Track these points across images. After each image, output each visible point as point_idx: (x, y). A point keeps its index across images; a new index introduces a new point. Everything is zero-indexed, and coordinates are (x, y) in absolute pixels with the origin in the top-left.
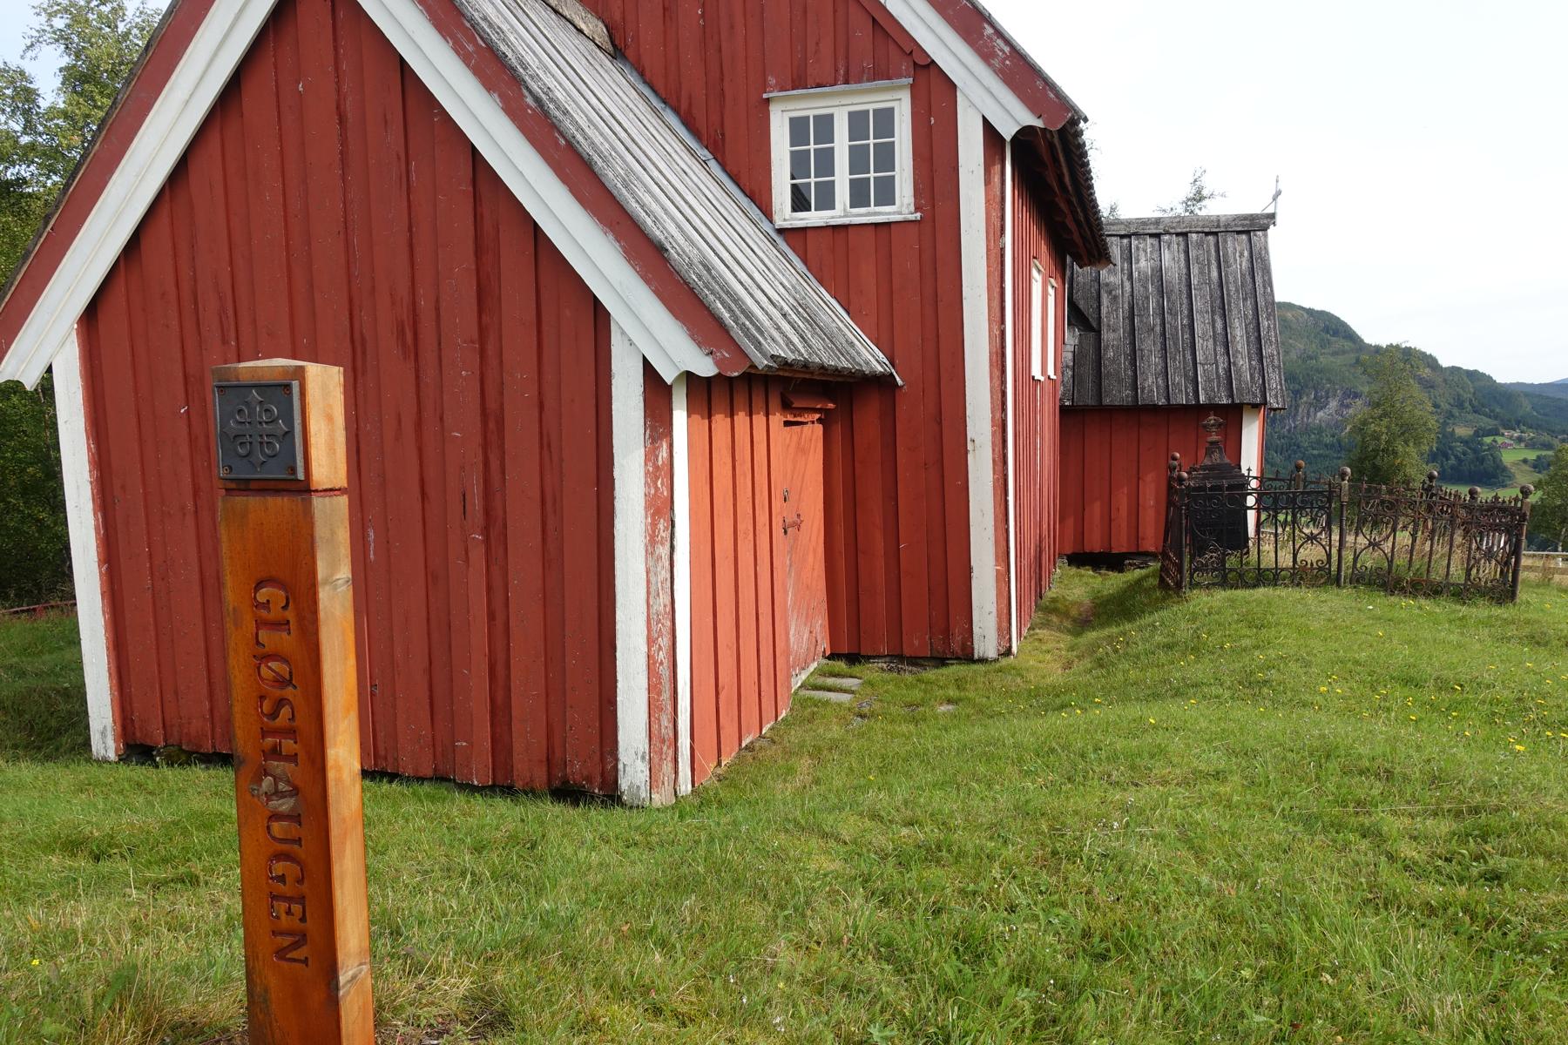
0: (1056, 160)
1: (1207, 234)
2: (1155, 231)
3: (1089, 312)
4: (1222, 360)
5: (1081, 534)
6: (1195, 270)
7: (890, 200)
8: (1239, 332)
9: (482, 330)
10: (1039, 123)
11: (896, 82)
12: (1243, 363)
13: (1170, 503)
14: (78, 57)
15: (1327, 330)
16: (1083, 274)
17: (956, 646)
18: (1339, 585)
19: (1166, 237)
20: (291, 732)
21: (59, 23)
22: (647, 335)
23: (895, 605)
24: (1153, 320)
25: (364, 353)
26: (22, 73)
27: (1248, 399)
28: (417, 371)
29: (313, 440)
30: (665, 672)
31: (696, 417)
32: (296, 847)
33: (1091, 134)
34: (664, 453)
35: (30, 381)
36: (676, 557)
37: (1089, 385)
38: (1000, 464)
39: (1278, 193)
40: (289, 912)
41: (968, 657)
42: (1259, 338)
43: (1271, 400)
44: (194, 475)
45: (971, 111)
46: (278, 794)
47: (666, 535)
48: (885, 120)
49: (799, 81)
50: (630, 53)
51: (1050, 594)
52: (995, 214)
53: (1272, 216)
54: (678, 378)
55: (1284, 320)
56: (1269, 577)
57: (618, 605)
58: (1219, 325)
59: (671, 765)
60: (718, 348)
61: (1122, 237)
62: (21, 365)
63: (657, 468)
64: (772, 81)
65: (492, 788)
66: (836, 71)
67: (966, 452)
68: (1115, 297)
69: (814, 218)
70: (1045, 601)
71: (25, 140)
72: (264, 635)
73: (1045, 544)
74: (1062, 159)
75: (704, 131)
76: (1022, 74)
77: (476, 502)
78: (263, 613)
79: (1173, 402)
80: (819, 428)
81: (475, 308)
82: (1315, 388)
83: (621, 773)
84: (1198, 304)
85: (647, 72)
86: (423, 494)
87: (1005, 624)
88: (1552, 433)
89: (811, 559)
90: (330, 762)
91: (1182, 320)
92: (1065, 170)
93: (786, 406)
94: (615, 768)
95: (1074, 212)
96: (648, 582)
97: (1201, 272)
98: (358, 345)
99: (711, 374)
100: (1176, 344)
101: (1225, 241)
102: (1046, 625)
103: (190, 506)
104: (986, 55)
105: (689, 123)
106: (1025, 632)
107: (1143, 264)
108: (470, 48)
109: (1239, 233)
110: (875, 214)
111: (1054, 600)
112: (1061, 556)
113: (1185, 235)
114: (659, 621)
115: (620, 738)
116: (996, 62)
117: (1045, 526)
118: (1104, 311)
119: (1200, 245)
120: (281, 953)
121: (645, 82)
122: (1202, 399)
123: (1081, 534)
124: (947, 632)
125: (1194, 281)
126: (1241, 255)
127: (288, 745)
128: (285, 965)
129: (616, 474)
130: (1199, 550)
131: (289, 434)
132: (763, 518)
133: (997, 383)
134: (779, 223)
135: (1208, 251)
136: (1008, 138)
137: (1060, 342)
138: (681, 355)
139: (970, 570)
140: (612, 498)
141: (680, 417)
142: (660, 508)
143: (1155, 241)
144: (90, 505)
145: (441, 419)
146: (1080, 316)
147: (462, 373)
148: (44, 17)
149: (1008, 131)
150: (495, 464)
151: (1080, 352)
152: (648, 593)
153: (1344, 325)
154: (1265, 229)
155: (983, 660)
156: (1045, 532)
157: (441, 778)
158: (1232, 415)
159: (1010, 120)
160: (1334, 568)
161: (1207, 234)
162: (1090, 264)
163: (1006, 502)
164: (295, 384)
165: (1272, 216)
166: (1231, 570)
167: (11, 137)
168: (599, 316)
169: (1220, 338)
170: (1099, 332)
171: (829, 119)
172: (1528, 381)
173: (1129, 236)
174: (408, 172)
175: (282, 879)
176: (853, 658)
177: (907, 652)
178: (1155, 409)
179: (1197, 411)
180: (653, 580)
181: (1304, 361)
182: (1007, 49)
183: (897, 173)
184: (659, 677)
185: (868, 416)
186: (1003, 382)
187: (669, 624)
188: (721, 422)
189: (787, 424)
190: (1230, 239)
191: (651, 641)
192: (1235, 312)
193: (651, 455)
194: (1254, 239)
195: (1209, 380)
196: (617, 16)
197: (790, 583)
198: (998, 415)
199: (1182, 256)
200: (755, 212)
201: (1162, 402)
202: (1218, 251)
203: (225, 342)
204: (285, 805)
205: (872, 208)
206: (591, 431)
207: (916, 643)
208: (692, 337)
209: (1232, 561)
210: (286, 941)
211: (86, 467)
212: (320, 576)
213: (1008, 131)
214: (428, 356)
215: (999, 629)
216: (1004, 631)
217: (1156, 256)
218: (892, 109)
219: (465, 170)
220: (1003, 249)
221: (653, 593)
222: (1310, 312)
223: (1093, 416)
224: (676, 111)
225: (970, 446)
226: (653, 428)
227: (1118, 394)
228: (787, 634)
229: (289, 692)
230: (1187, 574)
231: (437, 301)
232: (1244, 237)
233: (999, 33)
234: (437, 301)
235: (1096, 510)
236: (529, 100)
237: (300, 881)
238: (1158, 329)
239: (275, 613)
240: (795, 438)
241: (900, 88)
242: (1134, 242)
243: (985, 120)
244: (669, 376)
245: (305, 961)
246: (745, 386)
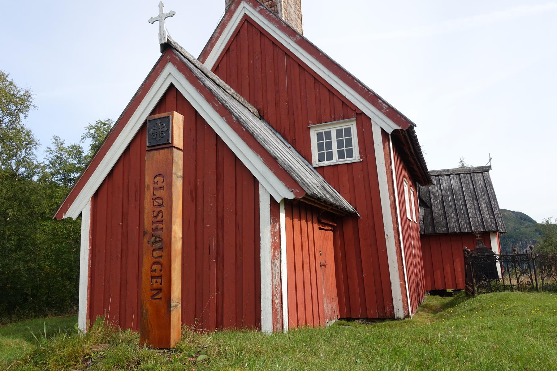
0: (408, 143)
1: (467, 174)
2: (448, 174)
3: (427, 201)
4: (479, 216)
5: (433, 283)
6: (464, 186)
7: (352, 156)
8: (484, 206)
9: (217, 190)
10: (400, 128)
11: (351, 119)
12: (487, 216)
13: (466, 263)
14: (96, 141)
15: (521, 219)
16: (423, 188)
17: (388, 313)
18: (538, 291)
21: (92, 131)
22: (272, 187)
23: (362, 297)
26: (79, 146)
27: (491, 229)
28: (196, 206)
29: (174, 132)
30: (278, 307)
31: (288, 218)
33: (419, 132)
34: (277, 228)
35: (74, 217)
36: (282, 264)
37: (430, 226)
38: (398, 244)
39: (491, 159)
41: (392, 318)
42: (492, 208)
44: (122, 246)
45: (377, 126)
47: (278, 256)
48: (348, 131)
49: (319, 121)
50: (265, 117)
51: (423, 303)
52: (388, 158)
53: (490, 167)
54: (282, 201)
55: (504, 216)
57: (262, 282)
58: (476, 204)
61: (436, 176)
62: (72, 213)
63: (275, 232)
64: (310, 122)
66: (331, 117)
67: (385, 239)
68: (436, 196)
69: (326, 163)
70: (423, 303)
71: (77, 166)
72: (156, 192)
73: (419, 282)
74: (409, 142)
75: (289, 138)
76: (392, 113)
77: (214, 248)
79: (462, 231)
80: (331, 233)
82: (521, 240)
85: (271, 123)
86: (196, 246)
87: (406, 305)
89: (331, 280)
90: (173, 230)
91: (461, 203)
92: (411, 146)
93: (319, 222)
95: (416, 163)
96: (272, 273)
97: (466, 186)
99: (293, 198)
101: (474, 176)
102: (423, 311)
103: (120, 256)
104: (380, 109)
105: (284, 137)
106: (415, 312)
107: (445, 185)
108: (217, 105)
109: (478, 173)
111: (425, 305)
112: (427, 291)
113: (459, 174)
114: (276, 288)
116: (383, 111)
117: (419, 276)
118: (432, 201)
119: (464, 177)
121: (270, 125)
122: (473, 230)
123: (433, 283)
124: (384, 308)
125: (464, 189)
126: (480, 180)
128: (154, 301)
129: (261, 235)
130: (479, 280)
131: (168, 130)
132: (312, 259)
133: (394, 214)
134: (314, 165)
135: (468, 179)
136: (390, 133)
137: (417, 212)
138: (283, 192)
139: (390, 283)
140: (260, 243)
141: (282, 216)
142: (276, 246)
143: (448, 177)
144: (88, 257)
145: (203, 221)
146: (423, 202)
148: (88, 130)
149: (389, 131)
151: (425, 215)
152: (272, 277)
153: (528, 216)
154: (488, 171)
155: (399, 319)
156: (419, 278)
158: (486, 236)
159: (390, 128)
160: (535, 285)
161: (467, 174)
162: (425, 185)
163: (402, 257)
164: (171, 116)
165: (490, 167)
166: (493, 286)
167: (74, 165)
168: (255, 182)
169: (477, 208)
170: (431, 208)
171: (330, 132)
173: (438, 176)
174: (196, 144)
176: (349, 319)
177: (369, 317)
178: (455, 234)
179: (470, 235)
180: (274, 272)
181: (515, 230)
182: (387, 106)
183: (353, 147)
184: (276, 309)
185: (349, 228)
186: (396, 214)
187: (280, 289)
188: (296, 221)
189: (320, 229)
190: (475, 175)
191: (273, 295)
192: (481, 199)
193: (273, 228)
194: (484, 175)
195: (475, 223)
196: (261, 107)
197: (323, 286)
198: (395, 226)
199: (459, 181)
200: (306, 162)
201: (458, 231)
202: (471, 179)
203: (136, 201)
205: (346, 159)
206: (253, 221)
207: (372, 313)
208: (286, 186)
209: (493, 284)
210: (155, 292)
211: (88, 244)
212: (174, 171)
213: (389, 131)
215: (404, 306)
216: (406, 307)
217: (449, 182)
218: (350, 128)
219: (213, 141)
220: (392, 169)
221: (274, 278)
222: (514, 212)
223: (433, 237)
224: (280, 133)
225: (386, 237)
226: (273, 219)
227: (441, 229)
228: (323, 305)
229: (162, 209)
230: (476, 289)
231: (203, 183)
233: (384, 102)
234: (203, 183)
235: (438, 274)
236: (234, 119)
237: (161, 271)
238: (453, 206)
239: (160, 185)
240: (323, 234)
241: (352, 121)
242: (440, 178)
244: (278, 200)
246: (305, 207)
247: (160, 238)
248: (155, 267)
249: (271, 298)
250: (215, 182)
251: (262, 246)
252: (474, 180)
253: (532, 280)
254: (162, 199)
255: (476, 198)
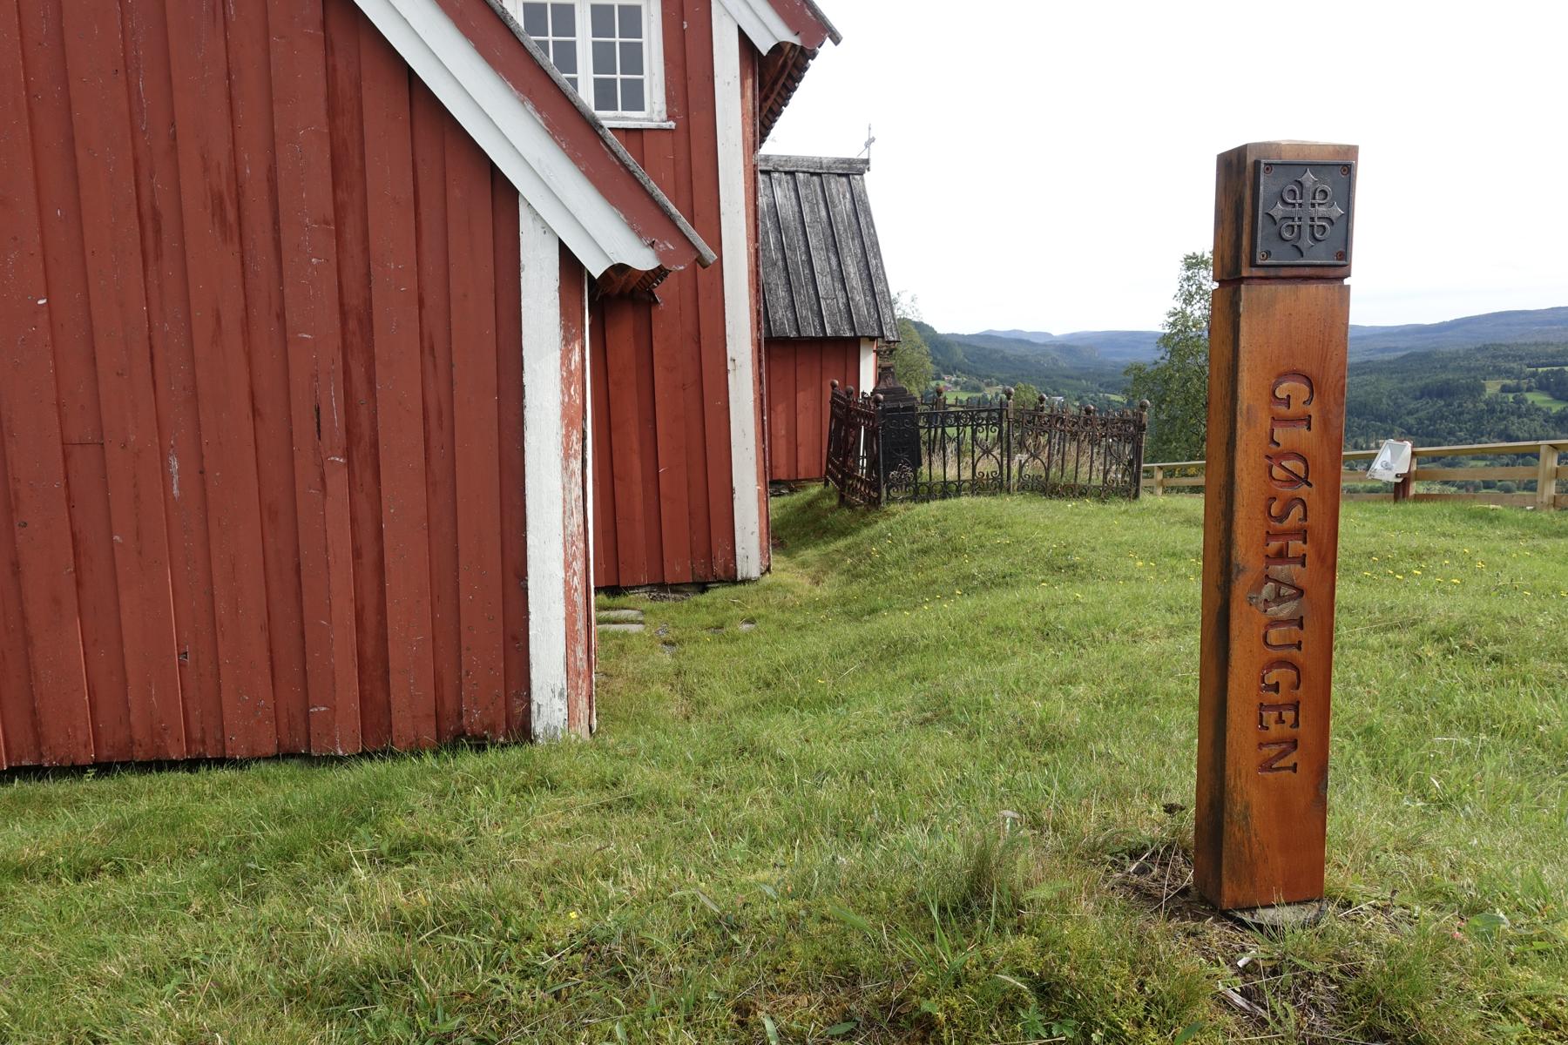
1: (812, 174)
4: (840, 294)
6: (806, 208)
7: (640, 106)
8: (852, 269)
12: (860, 298)
19: (776, 175)
20: (1303, 534)
24: (775, 255)
25: (158, 231)
27: (868, 332)
32: (1294, 651)
39: (872, 140)
40: (1280, 720)
41: (731, 579)
43: (887, 333)
45: (727, 20)
46: (1279, 599)
53: (867, 162)
56: (947, 490)
59: (586, 700)
60: (661, 241)
63: (570, 372)
65: (360, 755)
67: (727, 372)
77: (335, 418)
78: (1282, 409)
81: (330, 179)
83: (534, 715)
84: (813, 242)
86: (255, 411)
88: (979, 377)
91: (801, 257)
94: (528, 712)
97: (812, 211)
98: (149, 226)
99: (650, 268)
100: (799, 279)
110: (624, 118)
113: (792, 173)
115: (533, 676)
119: (807, 184)
120: (1267, 766)
122: (829, 332)
124: (709, 557)
125: (807, 219)
127: (1296, 546)
128: (1270, 775)
139: (732, 490)
145: (281, 316)
147: (312, 260)
149: (764, 45)
150: (358, 372)
154: (861, 174)
155: (745, 581)
157: (284, 755)
159: (767, 35)
161: (812, 174)
165: (867, 162)
169: (836, 274)
172: (960, 332)
175: (1276, 688)
177: (669, 580)
179: (838, 341)
183: (646, 77)
187: (582, 545)
195: (832, 314)
201: (793, 334)
204: (1285, 610)
207: (678, 569)
210: (1273, 751)
213: (764, 45)
214: (260, 236)
230: (884, 491)
232: (844, 179)
238: (780, 263)
239: (1296, 408)
243: (740, 29)
245: (1294, 768)
247: (1292, 586)
248: (1272, 677)
249: (561, 574)
250: (328, 172)
251: (529, 415)
252: (831, 195)
253: (1001, 467)
254: (1305, 462)
255: (835, 247)
